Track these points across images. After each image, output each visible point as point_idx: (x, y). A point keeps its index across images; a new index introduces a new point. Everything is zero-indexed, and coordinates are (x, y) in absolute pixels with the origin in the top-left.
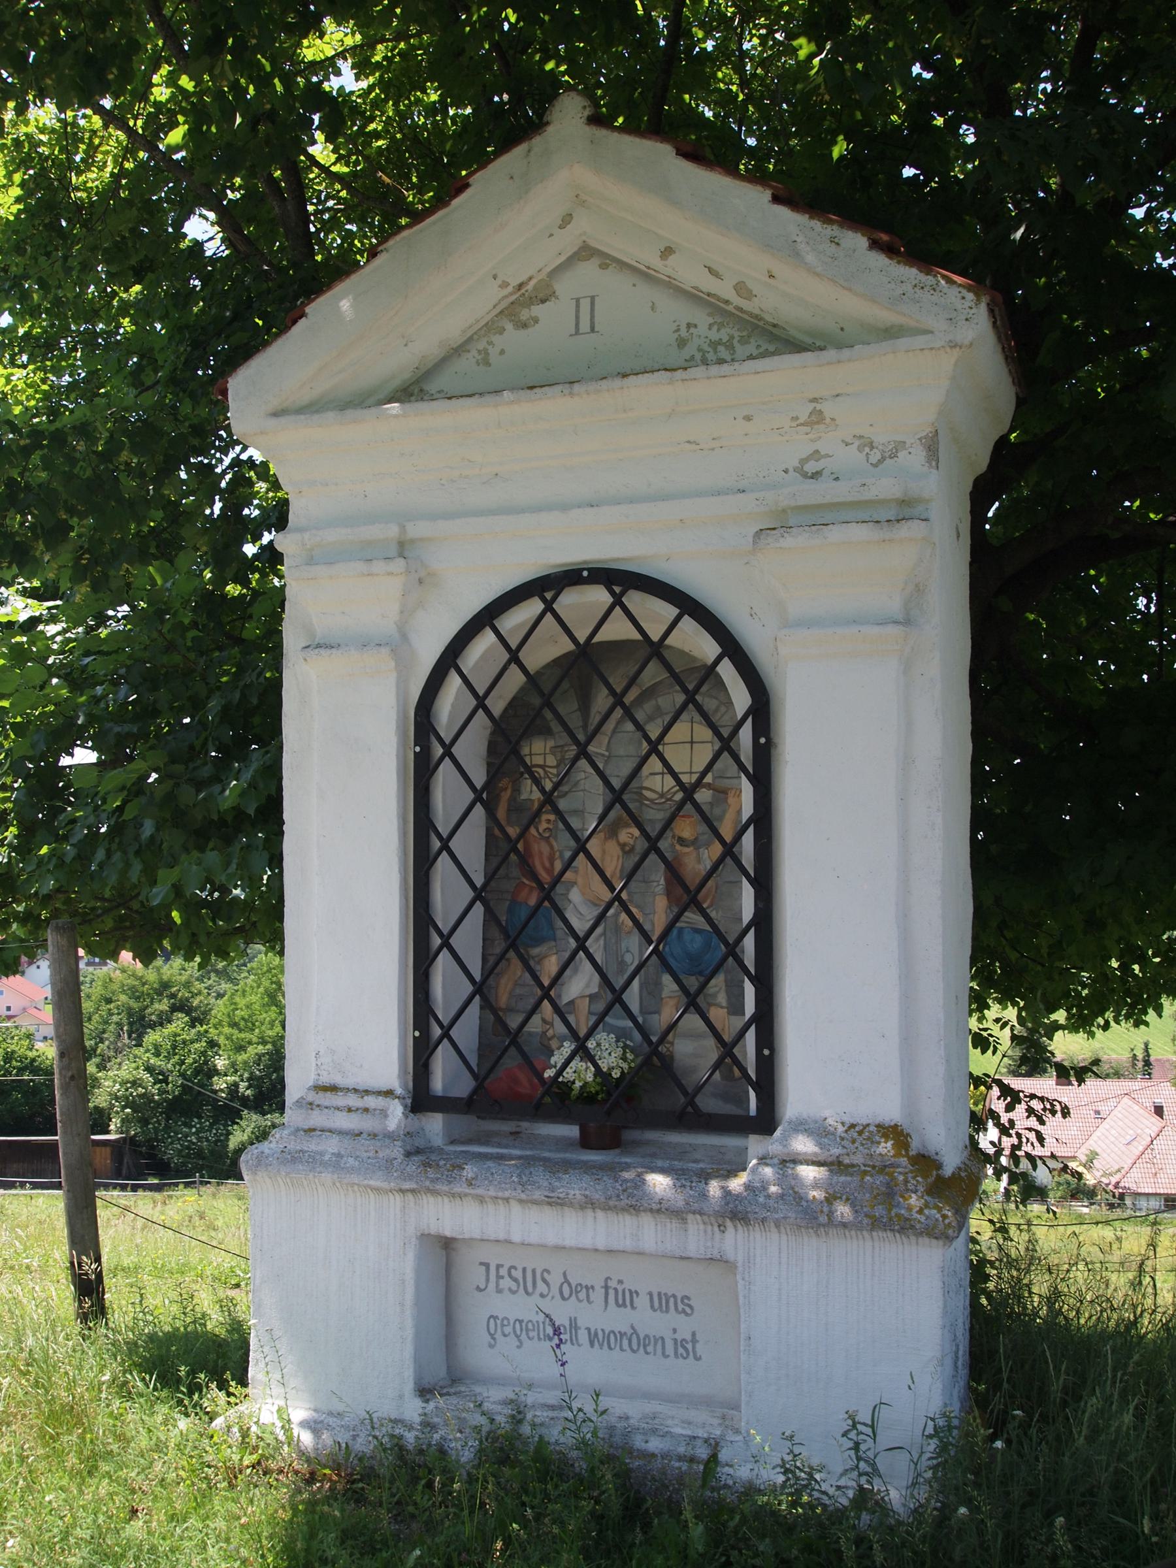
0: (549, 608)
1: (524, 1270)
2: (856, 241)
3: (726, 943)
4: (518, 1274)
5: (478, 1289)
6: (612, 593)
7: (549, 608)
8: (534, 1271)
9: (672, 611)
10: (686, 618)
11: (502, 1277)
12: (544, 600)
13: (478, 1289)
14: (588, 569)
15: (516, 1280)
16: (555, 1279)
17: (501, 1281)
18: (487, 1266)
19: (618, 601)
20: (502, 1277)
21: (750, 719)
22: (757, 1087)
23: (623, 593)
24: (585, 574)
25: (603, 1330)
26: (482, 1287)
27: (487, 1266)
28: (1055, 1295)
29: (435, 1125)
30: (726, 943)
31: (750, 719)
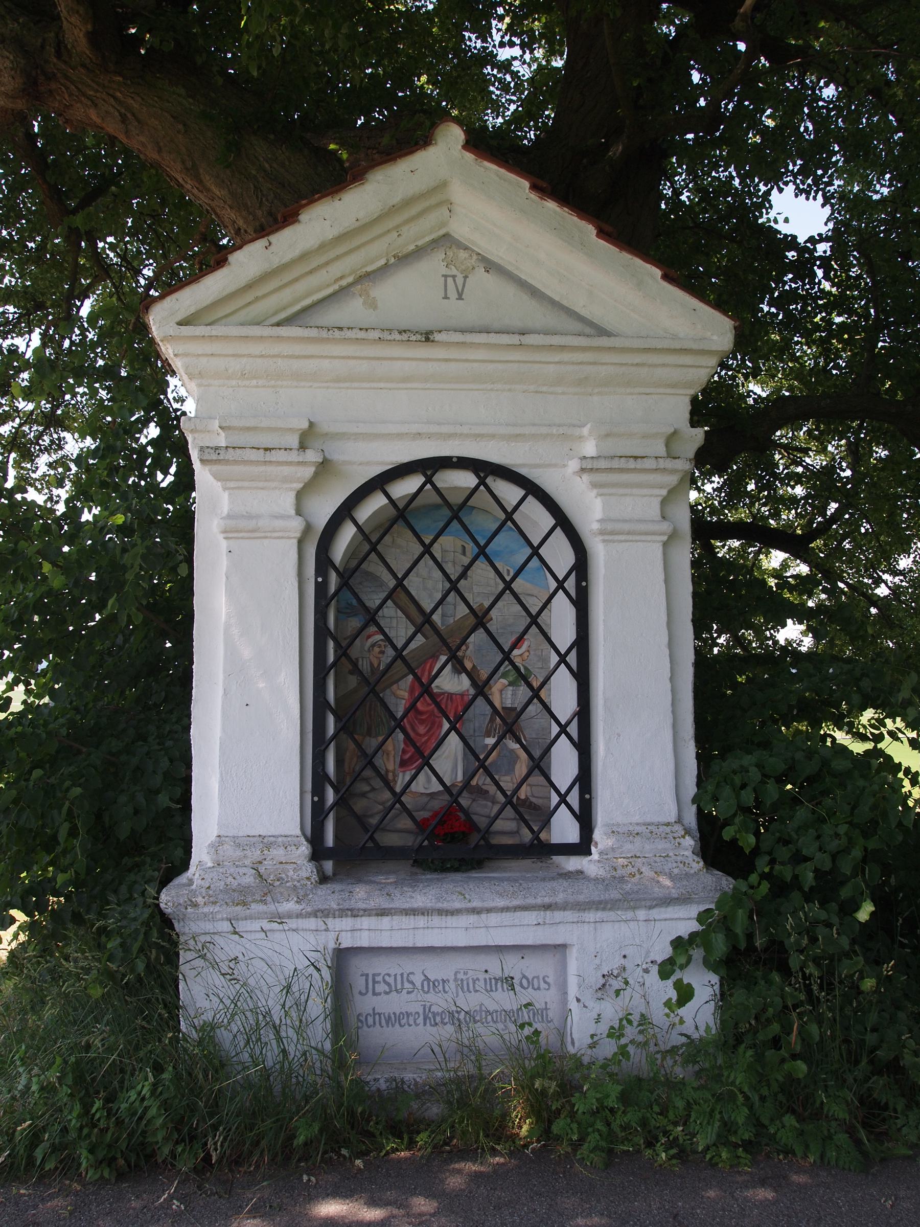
0: (429, 480)
1: (395, 975)
2: (690, 408)
3: (394, 647)
4: (391, 980)
5: (360, 993)
6: (478, 476)
7: (429, 480)
8: (402, 975)
9: (521, 493)
10: (530, 498)
11: (379, 982)
12: (425, 475)
13: (360, 993)
14: (587, 585)
15: (388, 984)
16: (418, 979)
17: (376, 985)
18: (367, 975)
19: (482, 482)
20: (379, 982)
21: (574, 573)
22: (326, 776)
23: (486, 477)
24: (584, 584)
25: (394, 1013)
26: (364, 991)
27: (367, 975)
28: (547, 1044)
29: (328, 866)
30: (394, 647)
31: (574, 573)
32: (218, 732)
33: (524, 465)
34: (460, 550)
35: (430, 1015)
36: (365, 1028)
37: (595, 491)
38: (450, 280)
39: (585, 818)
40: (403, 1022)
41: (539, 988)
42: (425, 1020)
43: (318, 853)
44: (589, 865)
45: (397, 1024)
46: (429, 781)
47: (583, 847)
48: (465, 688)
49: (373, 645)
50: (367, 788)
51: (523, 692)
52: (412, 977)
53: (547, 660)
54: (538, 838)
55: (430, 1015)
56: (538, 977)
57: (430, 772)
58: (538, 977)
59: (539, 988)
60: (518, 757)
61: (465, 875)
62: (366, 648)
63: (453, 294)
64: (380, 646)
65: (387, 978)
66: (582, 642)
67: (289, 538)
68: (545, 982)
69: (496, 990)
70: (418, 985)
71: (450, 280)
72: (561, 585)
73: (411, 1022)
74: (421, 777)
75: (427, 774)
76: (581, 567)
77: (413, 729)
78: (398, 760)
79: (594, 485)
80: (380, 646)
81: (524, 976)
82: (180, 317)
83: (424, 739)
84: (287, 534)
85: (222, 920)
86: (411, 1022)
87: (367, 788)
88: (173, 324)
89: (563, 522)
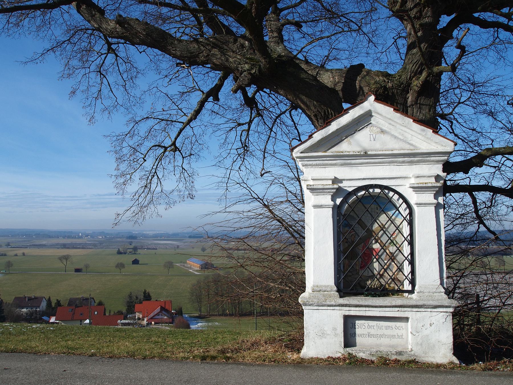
5: (351, 328)
10: (396, 194)
13: (351, 328)
27: (352, 323)
31: (409, 215)
32: (342, 286)
33: (390, 186)
34: (376, 209)
35: (370, 335)
36: (352, 337)
37: (414, 192)
38: (371, 136)
39: (413, 282)
40: (362, 336)
41: (400, 330)
42: (368, 336)
43: (339, 291)
44: (414, 296)
45: (361, 337)
46: (368, 272)
47: (412, 292)
48: (378, 247)
49: (352, 235)
50: (351, 274)
51: (395, 248)
52: (364, 324)
53: (402, 239)
54: (399, 288)
55: (370, 335)
56: (400, 326)
57: (369, 270)
58: (400, 326)
59: (400, 330)
60: (394, 266)
61: (452, 348)
62: (350, 236)
63: (372, 139)
64: (354, 235)
65: (358, 324)
66: (412, 234)
67: (330, 208)
68: (402, 328)
69: (388, 329)
70: (366, 326)
71: (371, 136)
72: (405, 219)
73: (365, 336)
74: (366, 271)
75: (368, 271)
76: (411, 214)
77: (364, 258)
78: (360, 267)
79: (414, 191)
80: (354, 235)
81: (396, 326)
82: (300, 151)
83: (367, 261)
84: (329, 207)
85: (315, 306)
86: (365, 336)
87: (351, 274)
88: (299, 153)
89: (406, 201)
